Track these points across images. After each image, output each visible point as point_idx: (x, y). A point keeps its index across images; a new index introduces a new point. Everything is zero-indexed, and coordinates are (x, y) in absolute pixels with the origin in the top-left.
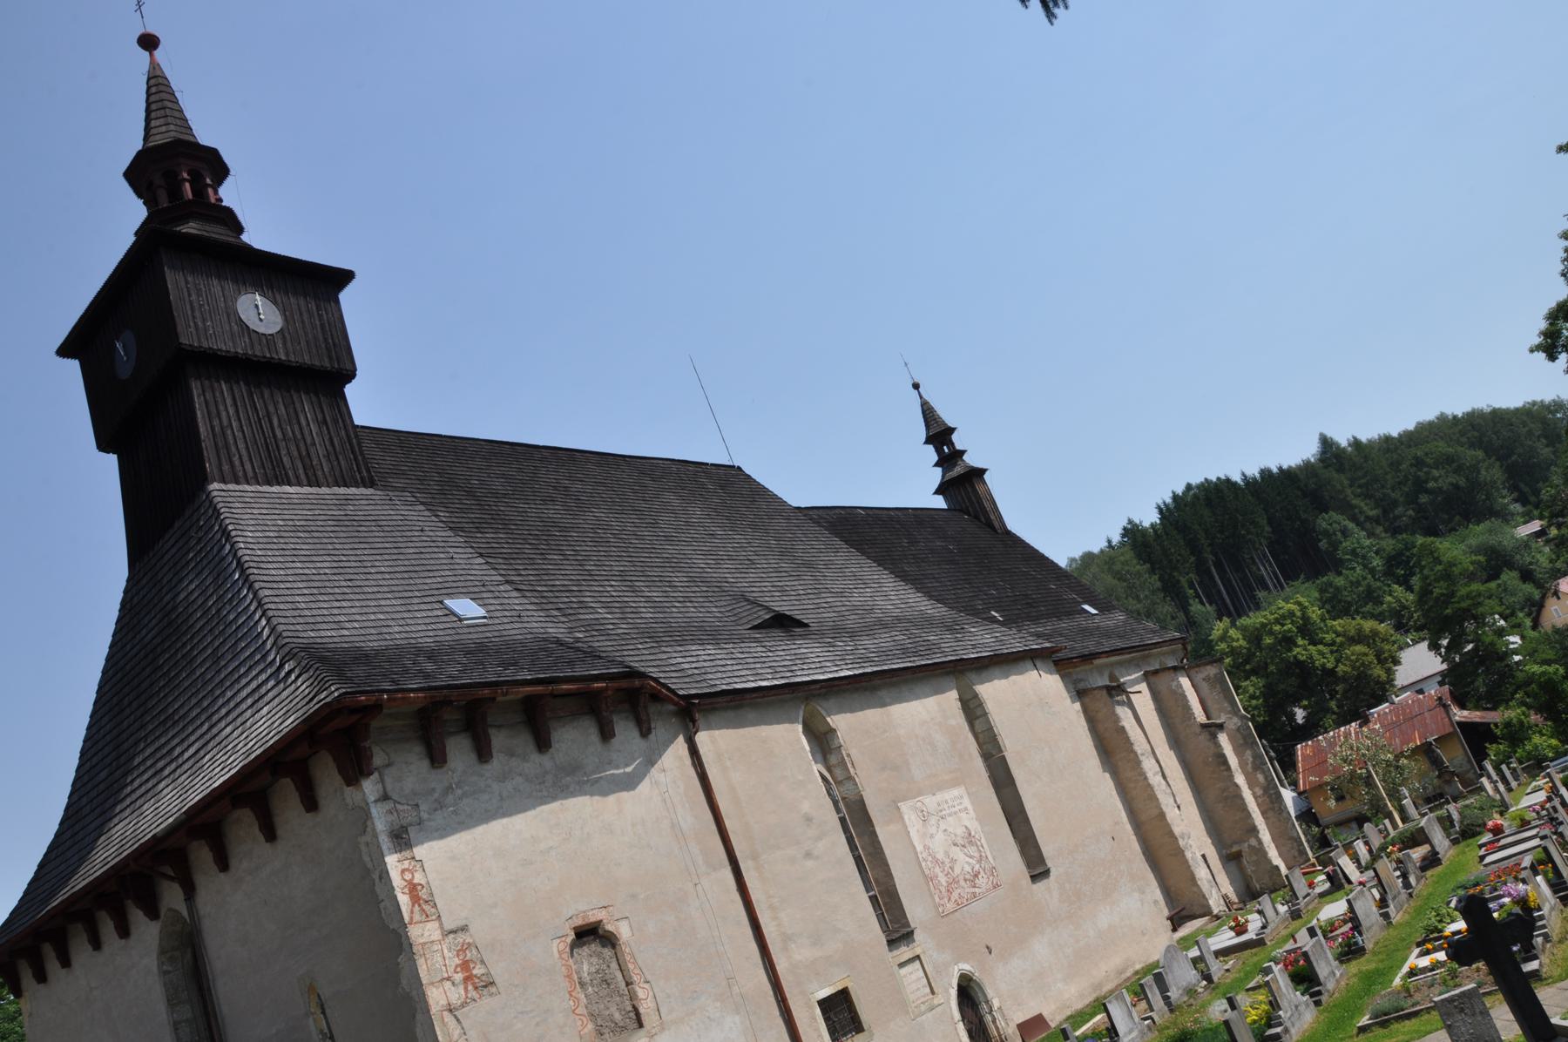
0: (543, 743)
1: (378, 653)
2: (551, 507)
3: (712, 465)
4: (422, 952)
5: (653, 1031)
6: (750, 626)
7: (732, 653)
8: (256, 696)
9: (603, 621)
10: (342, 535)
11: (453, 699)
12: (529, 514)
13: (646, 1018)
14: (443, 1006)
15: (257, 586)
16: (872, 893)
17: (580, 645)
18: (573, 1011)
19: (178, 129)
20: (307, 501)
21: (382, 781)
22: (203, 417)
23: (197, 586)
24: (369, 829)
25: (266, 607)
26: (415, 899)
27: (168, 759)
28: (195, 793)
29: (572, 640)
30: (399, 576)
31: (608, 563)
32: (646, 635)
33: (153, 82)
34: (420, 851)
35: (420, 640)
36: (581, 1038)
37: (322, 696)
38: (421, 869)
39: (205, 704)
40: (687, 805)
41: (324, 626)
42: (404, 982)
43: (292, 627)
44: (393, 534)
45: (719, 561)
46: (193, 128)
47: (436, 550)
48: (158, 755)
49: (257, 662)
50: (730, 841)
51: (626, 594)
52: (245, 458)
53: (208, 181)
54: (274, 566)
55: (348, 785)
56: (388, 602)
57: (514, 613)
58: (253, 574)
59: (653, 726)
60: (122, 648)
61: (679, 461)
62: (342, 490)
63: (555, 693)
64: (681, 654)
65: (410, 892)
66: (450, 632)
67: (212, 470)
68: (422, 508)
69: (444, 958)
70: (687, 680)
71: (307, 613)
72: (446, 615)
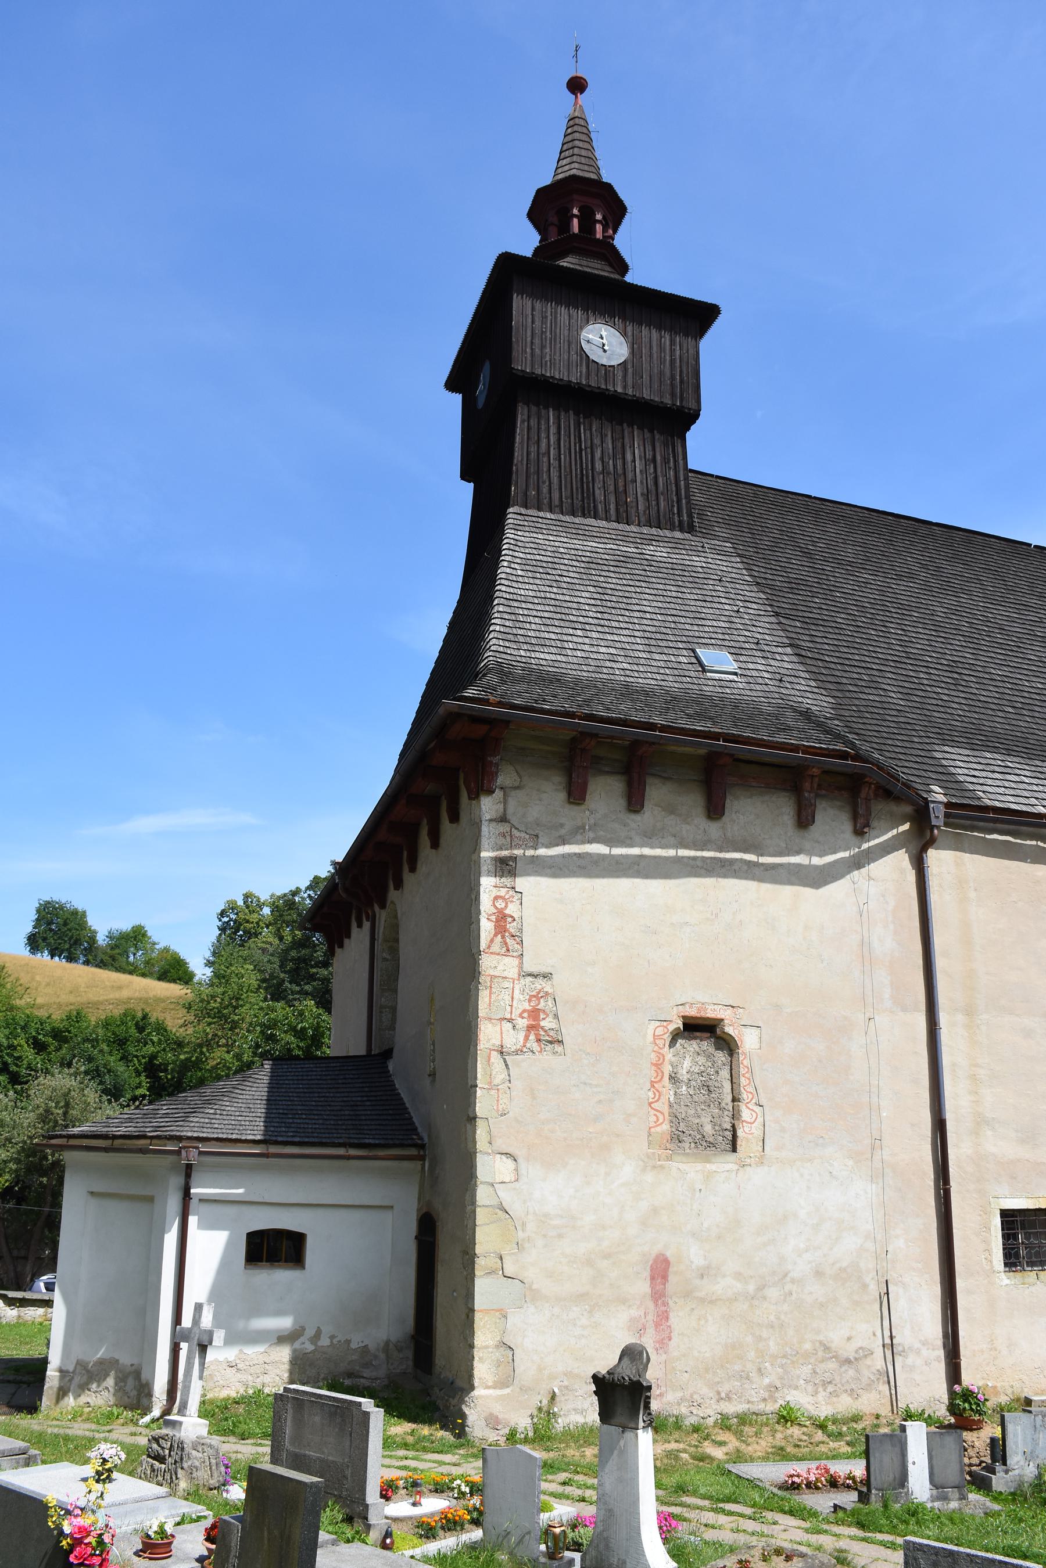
0: (715, 810)
4: (488, 984)
5: (748, 1161)
14: (494, 1045)
18: (650, 1104)
21: (505, 803)
22: (522, 443)
34: (523, 883)
36: (650, 1135)
38: (518, 902)
40: (891, 927)
58: (500, 590)
65: (497, 921)
67: (516, 493)
69: (512, 998)
72: (692, 664)
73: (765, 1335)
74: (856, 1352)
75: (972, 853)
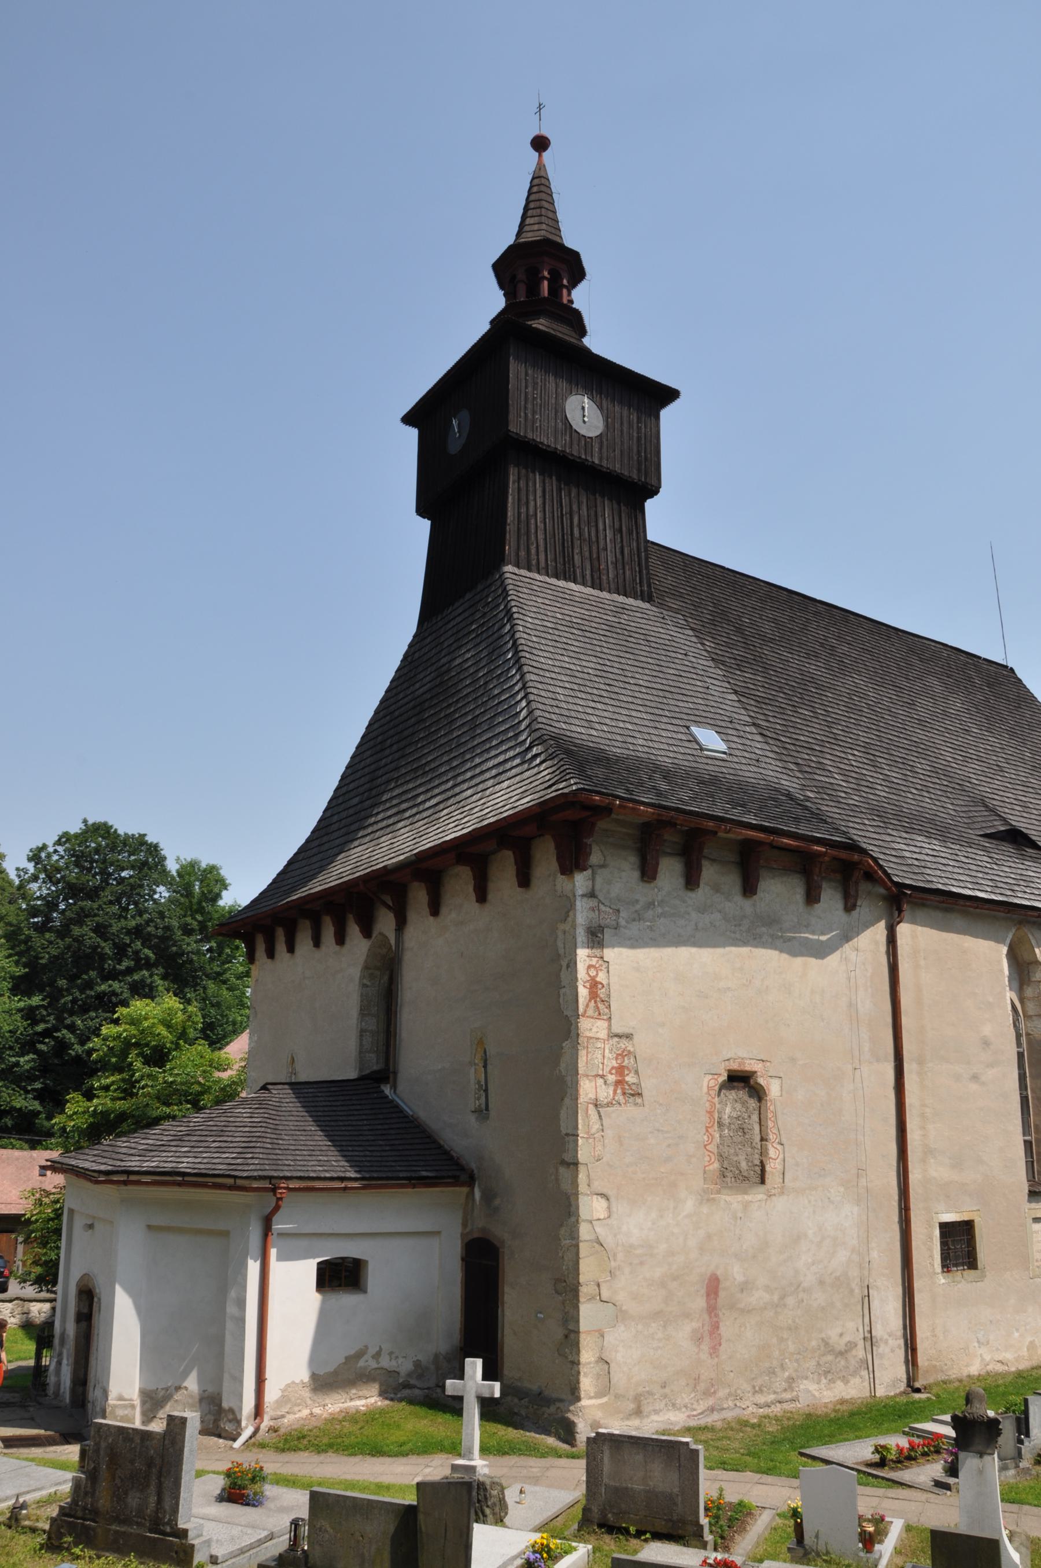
1: (618, 760)
2: (814, 662)
3: (985, 659)
6: (982, 833)
7: (957, 855)
8: (501, 769)
9: (836, 787)
10: (611, 640)
11: (678, 822)
12: (791, 664)
13: (770, 1177)
14: (590, 1099)
15: (526, 669)
16: (1028, 1138)
17: (808, 804)
18: (705, 1146)
19: (549, 229)
20: (588, 602)
21: (593, 879)
22: (513, 503)
23: (472, 656)
24: (570, 919)
25: (529, 690)
26: (593, 995)
27: (411, 804)
28: (428, 840)
29: (802, 798)
30: (655, 692)
31: (855, 732)
32: (876, 812)
33: (536, 181)
34: (609, 953)
35: (660, 758)
36: (705, 1172)
37: (561, 785)
38: (606, 970)
39: (455, 764)
41: (577, 722)
42: (563, 1066)
43: (547, 715)
44: (659, 652)
45: (967, 759)
46: (562, 229)
47: (695, 676)
48: (404, 798)
49: (509, 739)
50: (901, 1038)
51: (866, 767)
52: (542, 548)
53: (565, 282)
54: (545, 654)
55: (562, 874)
56: (639, 715)
57: (753, 756)
59: (859, 903)
60: (396, 695)
61: (951, 647)
62: (621, 599)
63: (775, 844)
64: (905, 841)
65: (591, 988)
66: (690, 758)
67: (510, 552)
68: (691, 633)
69: (604, 1057)
70: (904, 868)
71: (564, 705)
72: (690, 741)
73: (785, 1336)
74: (846, 1345)
75: (922, 926)
